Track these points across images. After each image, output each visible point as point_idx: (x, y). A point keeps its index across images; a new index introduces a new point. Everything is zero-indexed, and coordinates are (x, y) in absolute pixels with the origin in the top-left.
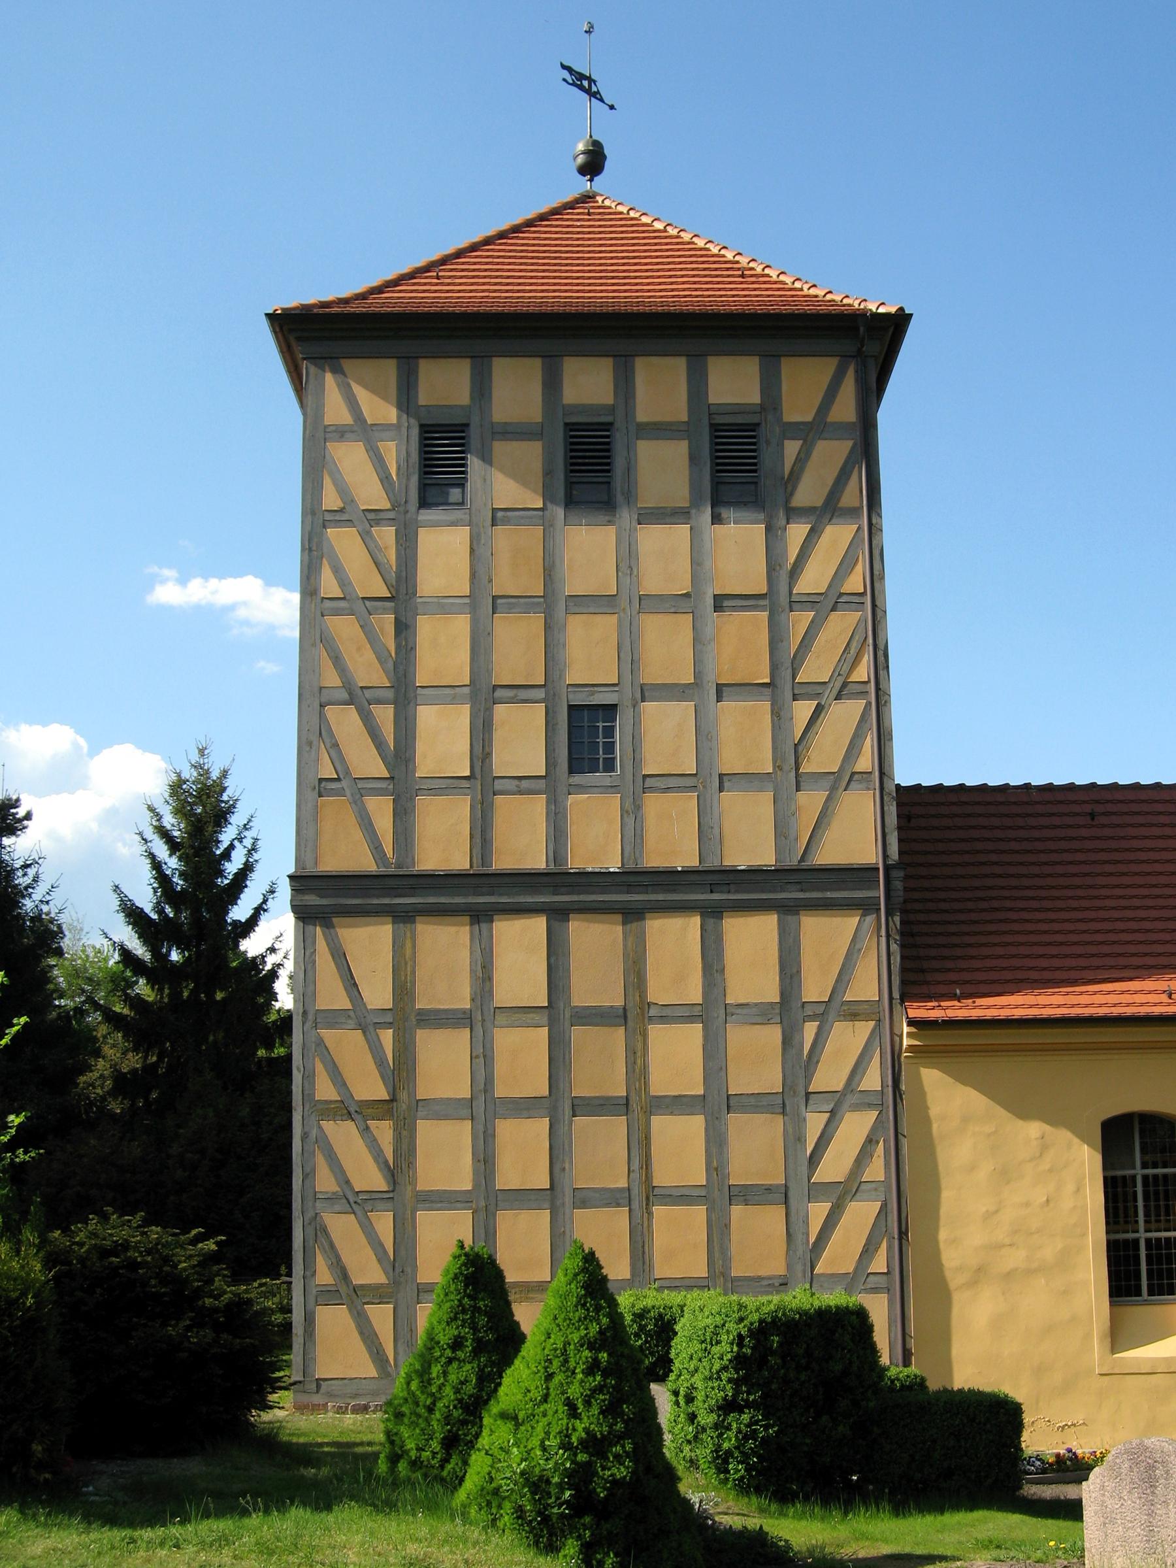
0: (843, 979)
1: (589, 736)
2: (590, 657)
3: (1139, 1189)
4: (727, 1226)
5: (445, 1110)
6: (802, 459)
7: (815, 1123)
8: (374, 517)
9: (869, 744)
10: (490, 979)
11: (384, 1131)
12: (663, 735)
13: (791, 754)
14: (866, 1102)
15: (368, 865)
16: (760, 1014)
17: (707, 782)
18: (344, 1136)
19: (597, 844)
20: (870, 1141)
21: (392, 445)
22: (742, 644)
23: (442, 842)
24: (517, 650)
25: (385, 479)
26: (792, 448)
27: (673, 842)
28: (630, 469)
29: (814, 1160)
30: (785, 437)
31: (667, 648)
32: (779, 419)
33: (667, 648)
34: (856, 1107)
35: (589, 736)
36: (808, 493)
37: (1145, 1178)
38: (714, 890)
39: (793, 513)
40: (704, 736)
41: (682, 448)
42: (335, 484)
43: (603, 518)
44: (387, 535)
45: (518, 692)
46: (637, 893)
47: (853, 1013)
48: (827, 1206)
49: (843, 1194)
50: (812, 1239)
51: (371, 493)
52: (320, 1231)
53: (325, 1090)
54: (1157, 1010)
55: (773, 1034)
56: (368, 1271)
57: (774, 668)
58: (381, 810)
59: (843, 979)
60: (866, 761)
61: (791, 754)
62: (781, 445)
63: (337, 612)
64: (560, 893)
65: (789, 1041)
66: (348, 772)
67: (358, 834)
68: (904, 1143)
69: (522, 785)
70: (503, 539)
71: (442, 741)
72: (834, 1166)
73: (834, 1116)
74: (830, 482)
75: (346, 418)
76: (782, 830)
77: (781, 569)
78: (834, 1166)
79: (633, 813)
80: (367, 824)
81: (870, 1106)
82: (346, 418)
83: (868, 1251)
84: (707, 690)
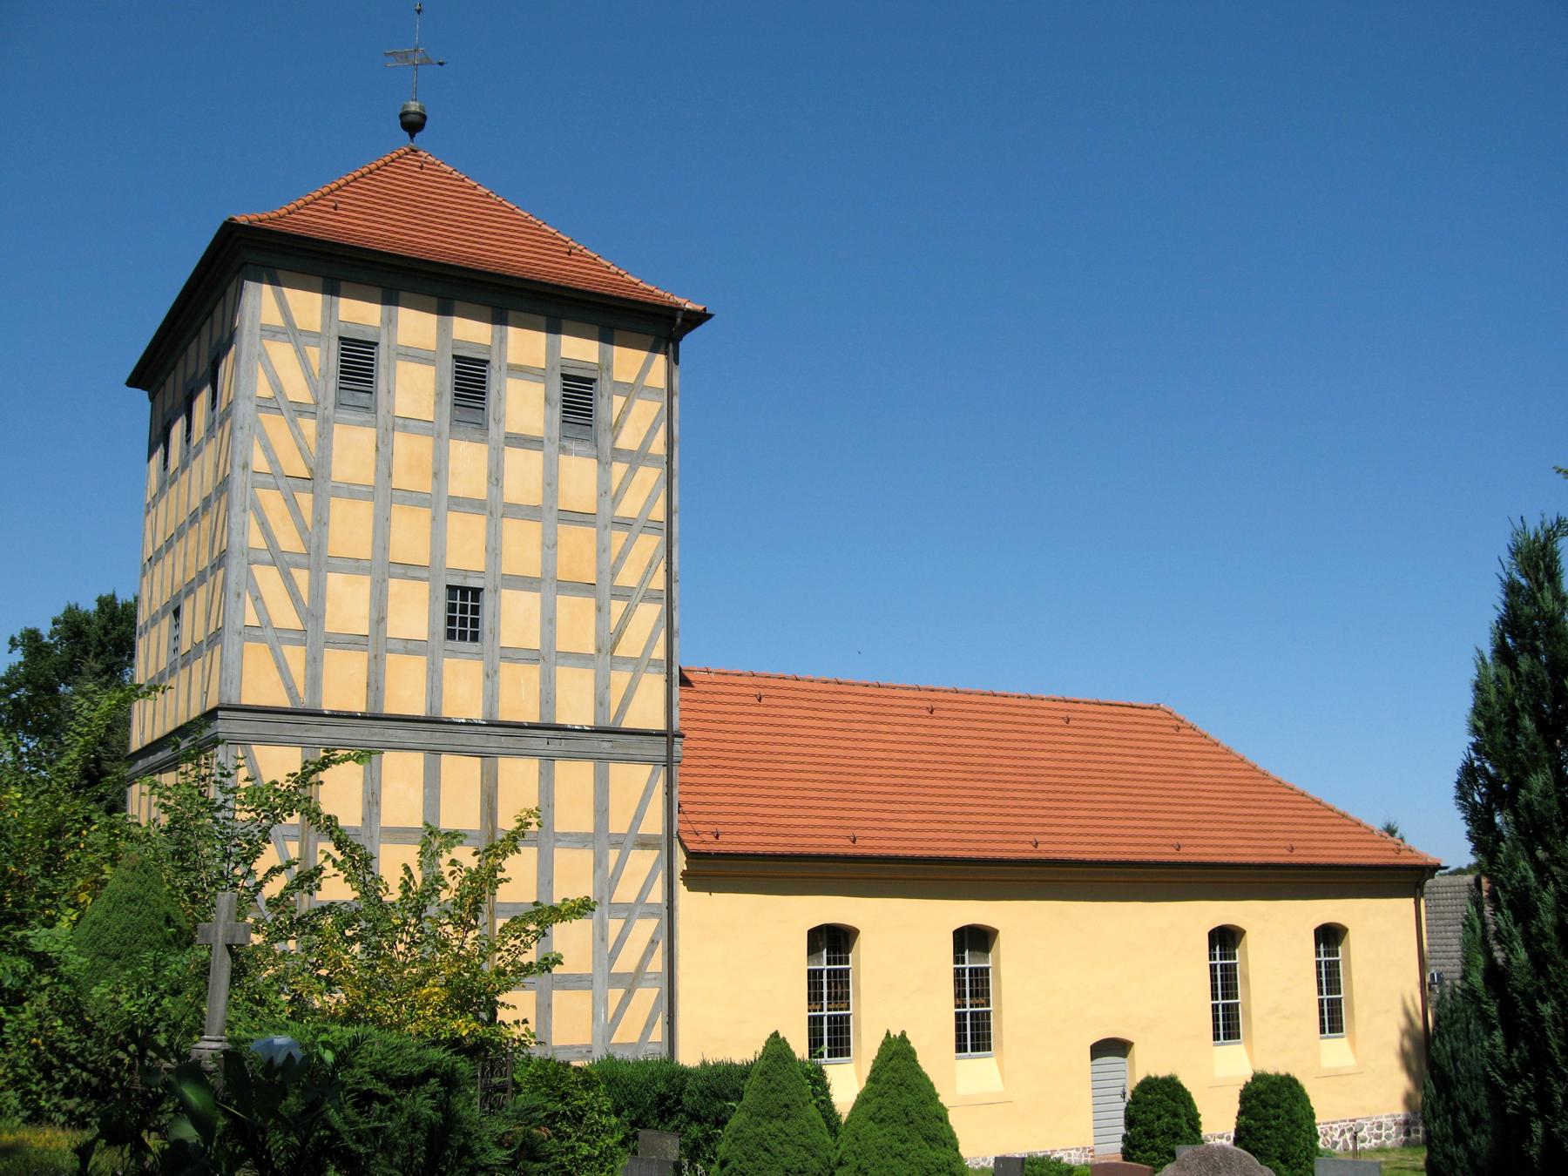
0: (638, 817)
1: (464, 612)
2: (466, 554)
3: (825, 980)
4: (550, 1006)
5: (352, 492)
6: (625, 412)
7: (615, 926)
8: (300, 410)
9: (660, 1021)
10: (378, 803)
11: (305, 500)
12: (514, 617)
13: (608, 644)
14: (649, 597)
15: (284, 702)
16: (581, 840)
17: (545, 658)
18: (275, 426)
19: (463, 695)
20: (653, 942)
21: (316, 350)
22: (577, 624)
23: (344, 687)
24: (410, 536)
25: (309, 376)
26: (618, 402)
27: (520, 703)
28: (500, 398)
29: (613, 957)
30: (614, 459)
31: (522, 547)
32: (610, 378)
33: (522, 547)
34: (643, 916)
35: (464, 612)
36: (629, 439)
37: (829, 971)
38: (547, 736)
39: (618, 454)
40: (549, 621)
41: (538, 389)
42: (266, 372)
43: (478, 436)
44: (309, 426)
45: (409, 571)
46: (497, 735)
47: (645, 843)
48: (622, 991)
49: (631, 982)
50: (610, 1016)
51: (297, 389)
52: (264, 357)
53: (259, 462)
54: (840, 851)
55: (587, 856)
56: (289, 540)
57: (599, 572)
58: (295, 657)
59: (638, 817)
60: (659, 653)
61: (608, 644)
62: (610, 398)
63: (265, 486)
64: (433, 731)
65: (599, 863)
66: (270, 622)
67: (276, 676)
68: (676, 642)
69: (410, 647)
70: (401, 442)
71: (348, 603)
72: (627, 962)
73: (629, 994)
74: (644, 433)
75: (277, 320)
76: (601, 703)
77: (609, 495)
78: (627, 962)
79: (491, 675)
80: (282, 667)
81: (653, 915)
82: (277, 320)
83: (647, 887)
84: (549, 584)
